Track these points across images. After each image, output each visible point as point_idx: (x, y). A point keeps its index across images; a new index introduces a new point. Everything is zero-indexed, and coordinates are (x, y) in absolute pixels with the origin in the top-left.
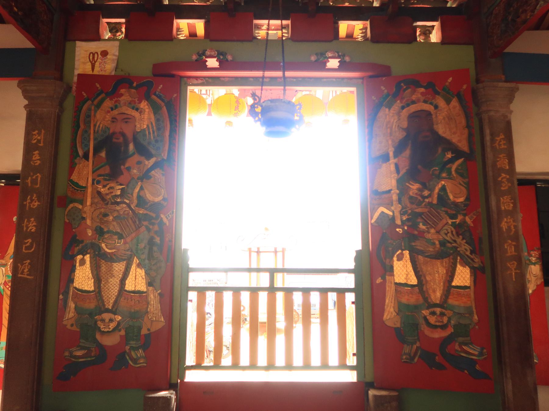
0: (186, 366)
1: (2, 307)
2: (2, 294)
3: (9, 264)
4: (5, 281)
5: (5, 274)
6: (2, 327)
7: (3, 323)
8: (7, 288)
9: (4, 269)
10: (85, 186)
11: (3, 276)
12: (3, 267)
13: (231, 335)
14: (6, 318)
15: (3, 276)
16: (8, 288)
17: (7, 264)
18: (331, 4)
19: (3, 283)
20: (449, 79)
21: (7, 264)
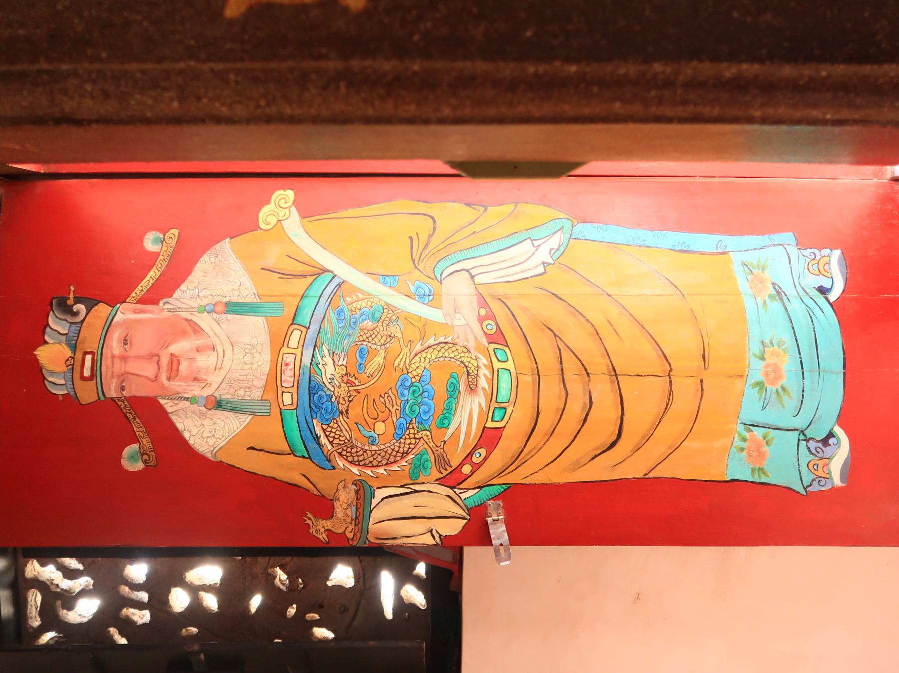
0: (842, 483)
1: (564, 485)
2: (500, 489)
3: (355, 470)
4: (441, 481)
5: (402, 486)
6: (654, 478)
7: (641, 476)
8: (473, 472)
9: (380, 494)
10: (832, 486)
11: (416, 491)
12: (372, 496)
13: (30, 620)
14: (87, 369)
15: (416, 491)
16: (473, 464)
17: (355, 483)
18: (279, 607)
19: (449, 492)
20: (46, 636)
21: (355, 483)
